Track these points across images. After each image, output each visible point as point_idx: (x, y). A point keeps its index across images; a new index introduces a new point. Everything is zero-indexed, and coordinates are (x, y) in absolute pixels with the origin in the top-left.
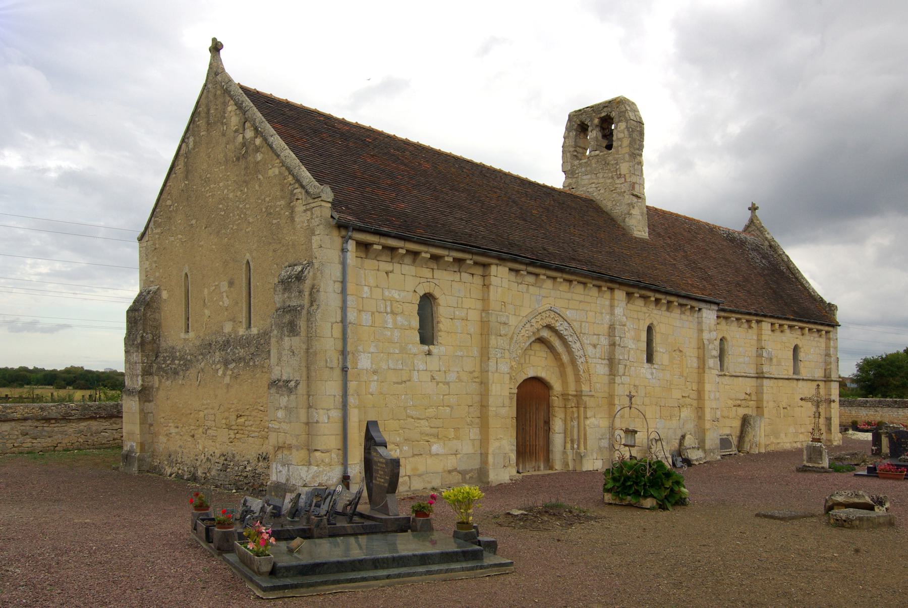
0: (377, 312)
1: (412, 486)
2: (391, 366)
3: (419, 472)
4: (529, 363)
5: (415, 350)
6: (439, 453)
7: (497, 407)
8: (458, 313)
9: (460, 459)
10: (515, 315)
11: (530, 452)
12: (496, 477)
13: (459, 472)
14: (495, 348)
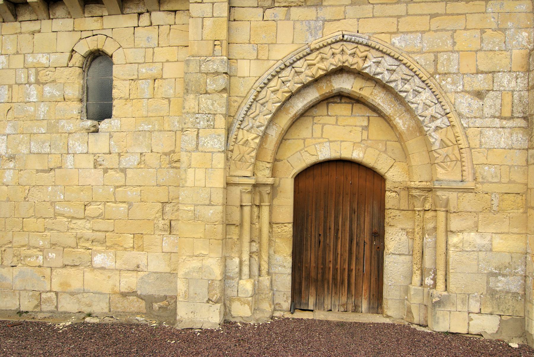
0: (16, 83)
1: (59, 306)
2: (34, 149)
3: (72, 289)
4: (322, 137)
5: (70, 127)
6: (106, 266)
7: (196, 205)
8: (144, 71)
9: (142, 278)
10: (257, 59)
11: (335, 279)
12: (191, 316)
13: (140, 297)
14: (194, 113)
